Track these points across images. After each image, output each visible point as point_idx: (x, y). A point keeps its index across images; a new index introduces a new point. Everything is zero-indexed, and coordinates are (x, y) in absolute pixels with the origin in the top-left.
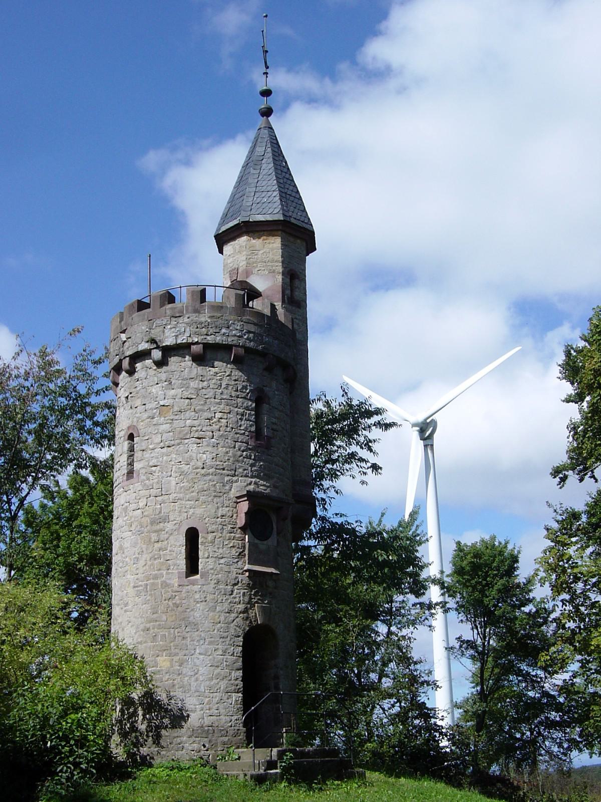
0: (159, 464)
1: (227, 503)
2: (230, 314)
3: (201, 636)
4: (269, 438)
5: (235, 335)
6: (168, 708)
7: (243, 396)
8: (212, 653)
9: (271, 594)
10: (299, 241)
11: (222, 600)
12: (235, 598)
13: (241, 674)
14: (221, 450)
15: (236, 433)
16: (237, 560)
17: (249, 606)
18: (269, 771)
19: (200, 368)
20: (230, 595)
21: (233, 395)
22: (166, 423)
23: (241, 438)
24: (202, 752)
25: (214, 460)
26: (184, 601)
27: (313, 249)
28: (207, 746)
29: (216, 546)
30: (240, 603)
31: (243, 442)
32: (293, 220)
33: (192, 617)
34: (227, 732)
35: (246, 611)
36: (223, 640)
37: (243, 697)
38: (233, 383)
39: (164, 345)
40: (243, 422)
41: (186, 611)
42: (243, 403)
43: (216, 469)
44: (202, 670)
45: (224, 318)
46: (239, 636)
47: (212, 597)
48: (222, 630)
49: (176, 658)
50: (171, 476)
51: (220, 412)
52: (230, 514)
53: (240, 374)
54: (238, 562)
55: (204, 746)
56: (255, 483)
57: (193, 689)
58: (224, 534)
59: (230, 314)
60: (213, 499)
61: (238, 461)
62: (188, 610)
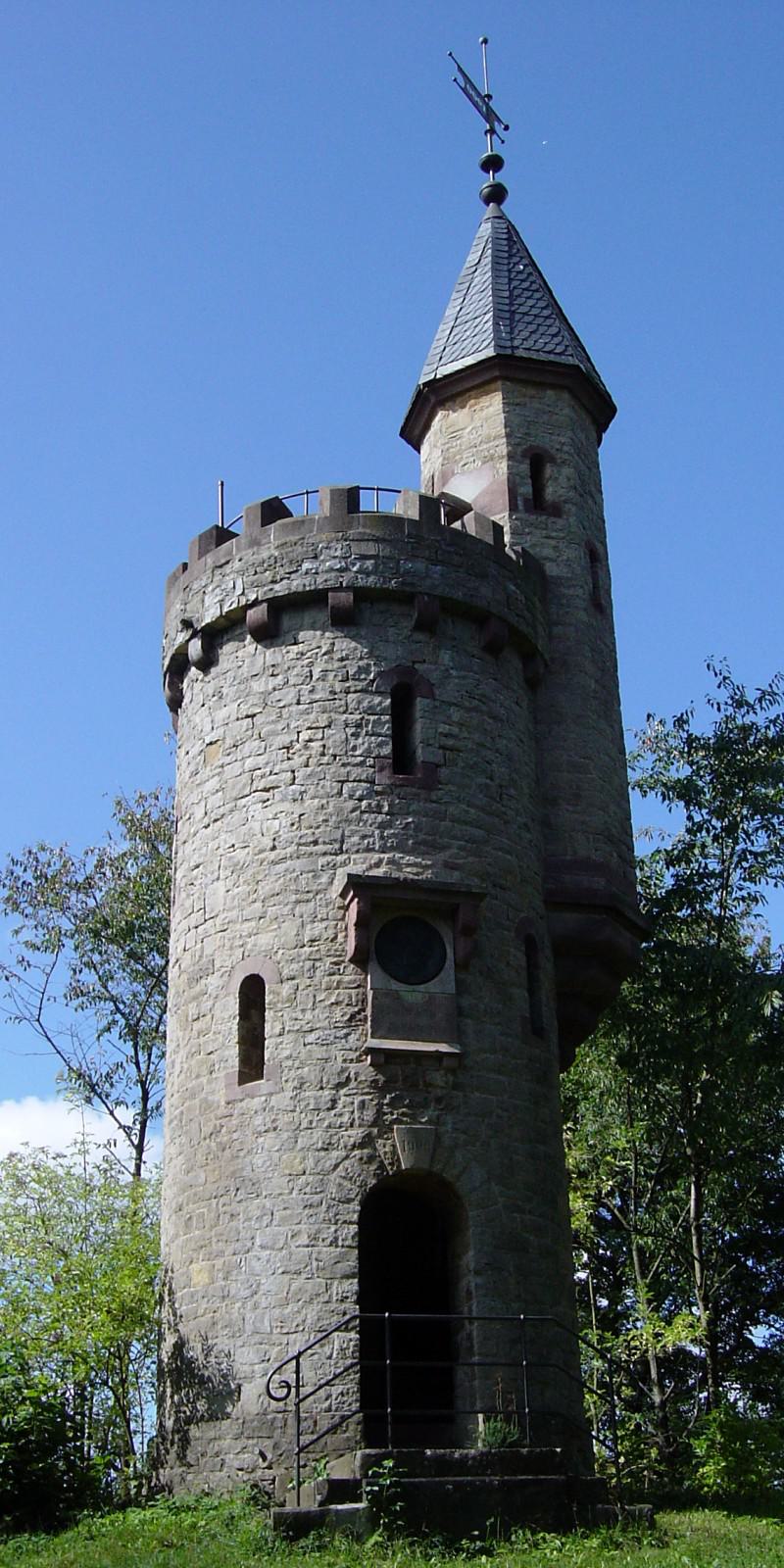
0: (201, 860)
1: (322, 913)
2: (320, 530)
3: (264, 1207)
4: (432, 768)
5: (331, 570)
6: (203, 1375)
7: (359, 688)
8: (286, 1243)
9: (439, 1100)
10: (550, 393)
11: (311, 1122)
12: (341, 1115)
13: (356, 1287)
14: (311, 804)
15: (344, 765)
16: (345, 1031)
17: (375, 1130)
18: (333, 1507)
19: (269, 652)
20: (328, 1109)
21: (338, 690)
22: (213, 776)
23: (356, 772)
24: (259, 1473)
25: (295, 827)
26: (235, 1136)
27: (611, 410)
28: (269, 1456)
29: (299, 1008)
30: (352, 1125)
31: (360, 781)
32: (520, 353)
33: (249, 1168)
34: (315, 1422)
35: (367, 1142)
36: (311, 1211)
37: (361, 1340)
38: (337, 665)
39: (203, 624)
40: (360, 740)
41: (237, 1157)
42: (359, 702)
43: (299, 845)
44: (267, 1283)
45: (306, 541)
46: (349, 1201)
47: (287, 1118)
48: (308, 1190)
49: (219, 1263)
50: (218, 879)
51: (309, 728)
52: (330, 933)
53: (353, 644)
54: (347, 1035)
55: (262, 1455)
56: (391, 862)
57: (249, 1328)
58: (316, 980)
59: (320, 530)
60: (293, 909)
61: (348, 821)
62: (242, 1154)
